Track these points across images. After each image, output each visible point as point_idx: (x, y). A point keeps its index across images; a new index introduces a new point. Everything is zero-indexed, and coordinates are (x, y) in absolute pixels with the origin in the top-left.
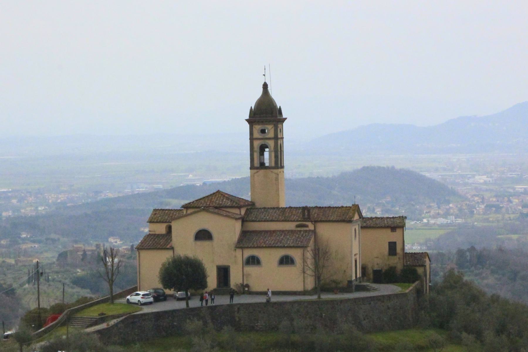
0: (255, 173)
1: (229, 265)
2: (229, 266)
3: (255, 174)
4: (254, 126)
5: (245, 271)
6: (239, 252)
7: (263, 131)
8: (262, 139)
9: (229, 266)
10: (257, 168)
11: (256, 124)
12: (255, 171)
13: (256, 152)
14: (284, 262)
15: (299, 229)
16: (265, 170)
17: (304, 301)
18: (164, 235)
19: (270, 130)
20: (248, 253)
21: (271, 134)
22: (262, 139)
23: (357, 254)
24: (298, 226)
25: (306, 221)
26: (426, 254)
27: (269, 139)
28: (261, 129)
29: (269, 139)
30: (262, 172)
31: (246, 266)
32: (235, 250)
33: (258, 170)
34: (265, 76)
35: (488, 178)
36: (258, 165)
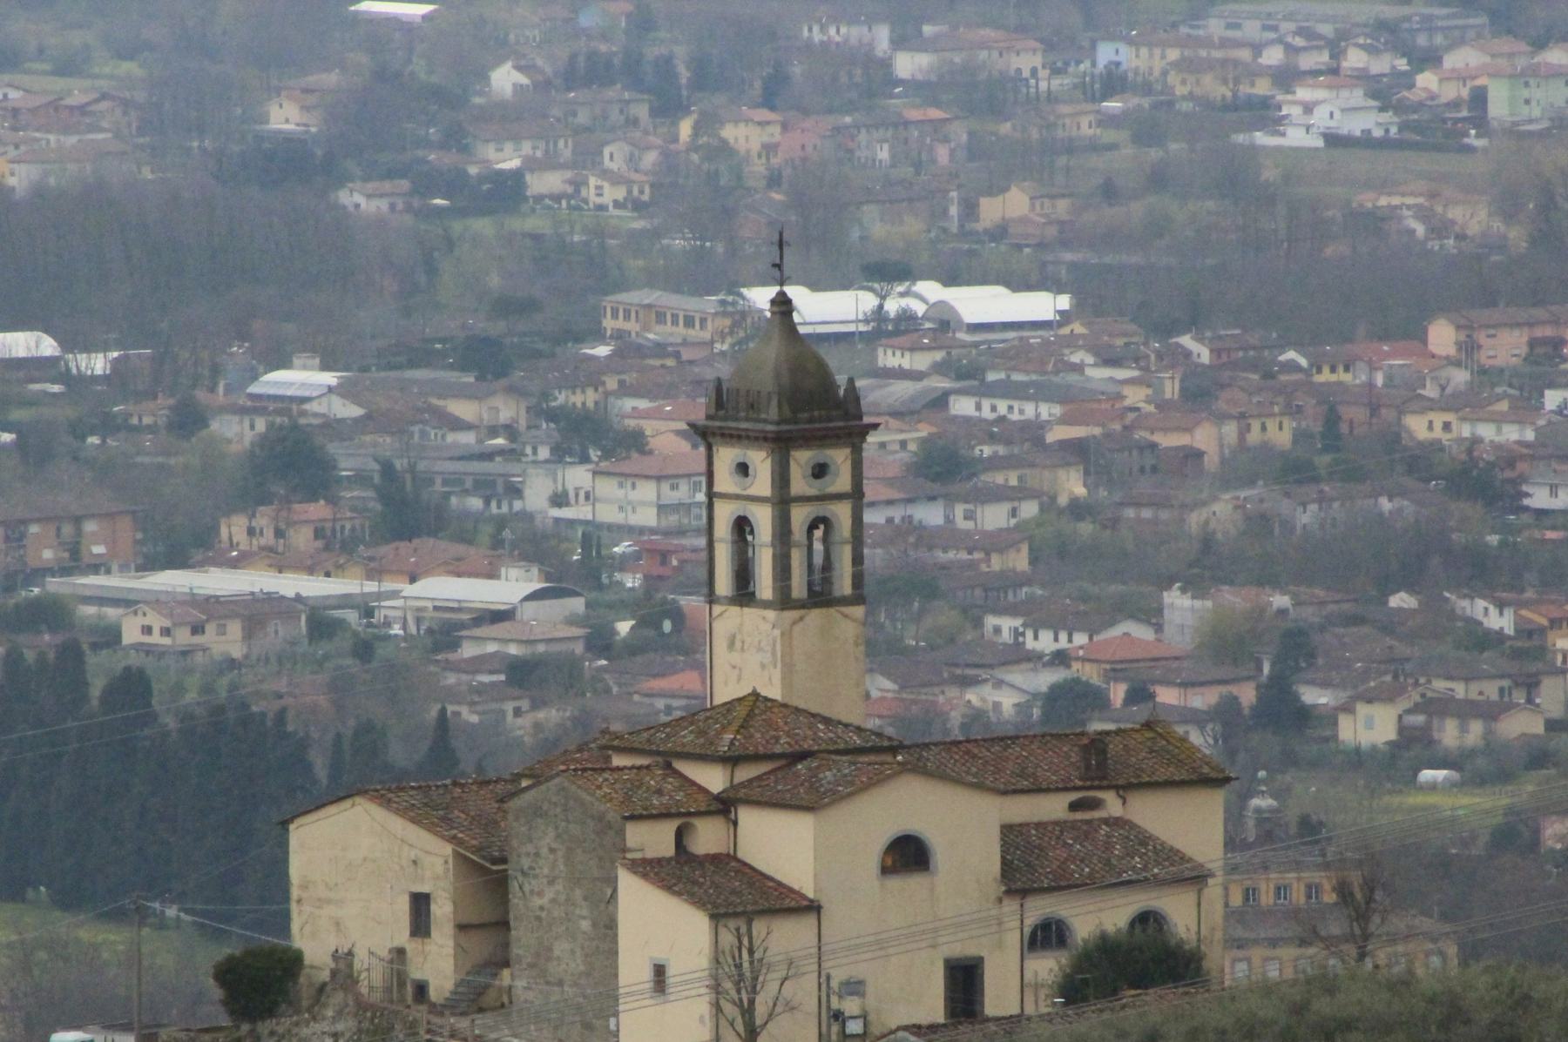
0: (794, 623)
1: (982, 955)
2: (981, 959)
4: (792, 453)
5: (1028, 975)
6: (1011, 906)
7: (743, 469)
9: (981, 959)
11: (800, 447)
12: (795, 614)
13: (798, 546)
14: (1039, 943)
15: (1079, 816)
16: (824, 610)
19: (839, 457)
20: (1039, 909)
21: (841, 481)
22: (737, 497)
24: (1074, 807)
26: (1137, 925)
27: (839, 497)
28: (749, 464)
29: (839, 497)
30: (815, 616)
31: (1031, 955)
32: (1000, 900)
33: (802, 612)
34: (780, 269)
35: (1007, 630)
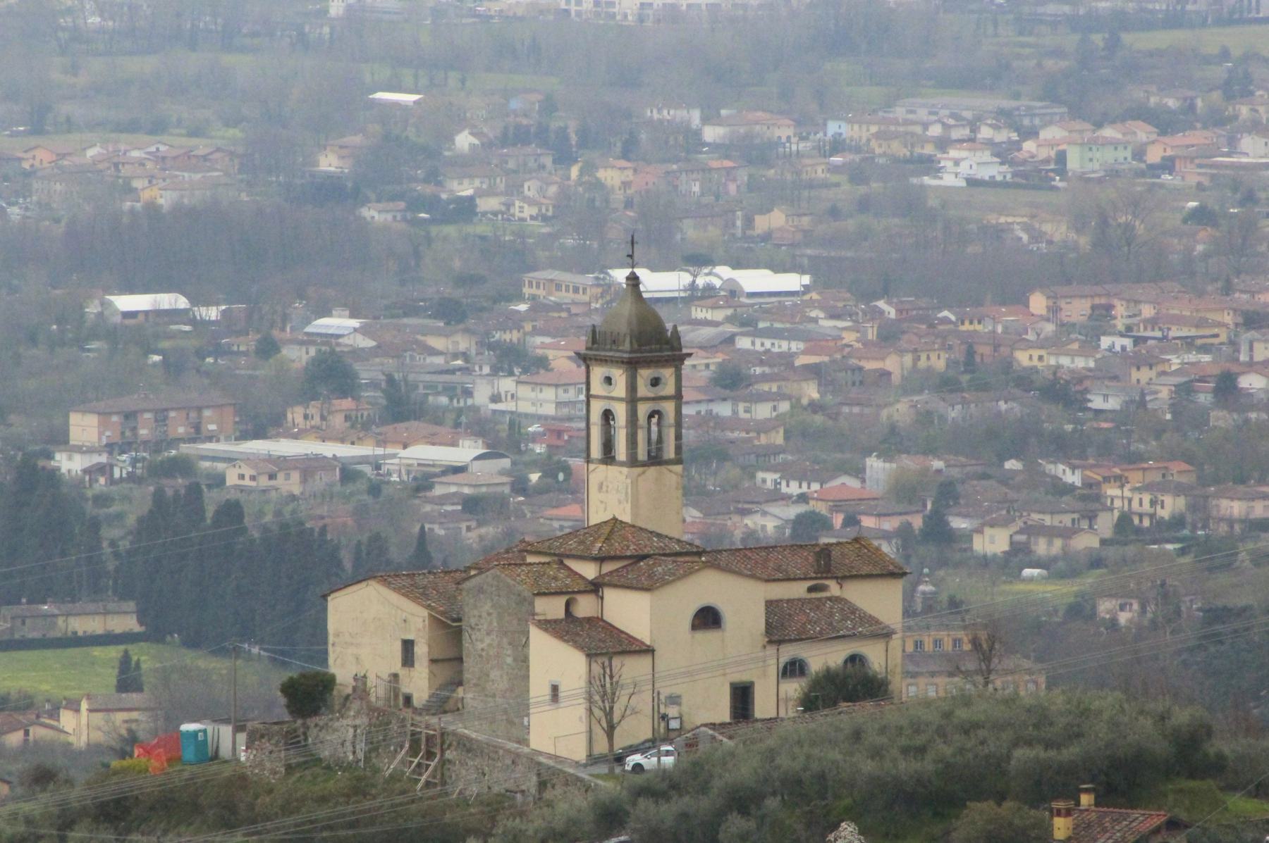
0: (639, 475)
1: (754, 679)
3: (640, 479)
6: (771, 650)
7: (608, 380)
8: (654, 399)
10: (644, 465)
12: (640, 470)
15: (814, 595)
17: (551, 763)
18: (562, 620)
20: (789, 652)
21: (669, 389)
22: (654, 399)
23: (125, 661)
24: (810, 590)
25: (822, 578)
30: (652, 471)
32: (764, 647)
36: (645, 458)
